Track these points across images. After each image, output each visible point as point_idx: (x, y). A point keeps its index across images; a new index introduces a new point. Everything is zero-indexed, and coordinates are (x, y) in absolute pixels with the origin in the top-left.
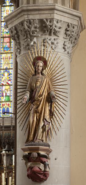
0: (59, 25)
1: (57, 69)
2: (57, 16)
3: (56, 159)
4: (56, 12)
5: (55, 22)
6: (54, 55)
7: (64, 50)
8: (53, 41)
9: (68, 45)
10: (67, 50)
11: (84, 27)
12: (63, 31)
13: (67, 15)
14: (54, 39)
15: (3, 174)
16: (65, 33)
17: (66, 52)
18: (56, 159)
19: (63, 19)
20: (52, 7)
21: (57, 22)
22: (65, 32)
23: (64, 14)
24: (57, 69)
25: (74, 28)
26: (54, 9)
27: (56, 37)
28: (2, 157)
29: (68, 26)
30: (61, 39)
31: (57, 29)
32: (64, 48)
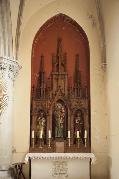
0: (5, 65)
1: (4, 85)
2: (4, 61)
3: (3, 127)
4: (3, 59)
5: (3, 64)
6: (3, 79)
7: (9, 77)
8: (3, 73)
9: (11, 75)
10: (11, 77)
11: (21, 67)
12: (8, 68)
13: (9, 61)
14: (4, 72)
15: (69, 132)
16: (9, 69)
17: (10, 78)
18: (3, 127)
19: (7, 63)
20: (1, 57)
21: (5, 64)
22: (20, 71)
23: (8, 61)
24: (4, 85)
25: (14, 67)
26: (2, 58)
27: (4, 71)
28: (47, 131)
29: (11, 66)
30: (7, 72)
31: (4, 67)
32: (9, 76)
